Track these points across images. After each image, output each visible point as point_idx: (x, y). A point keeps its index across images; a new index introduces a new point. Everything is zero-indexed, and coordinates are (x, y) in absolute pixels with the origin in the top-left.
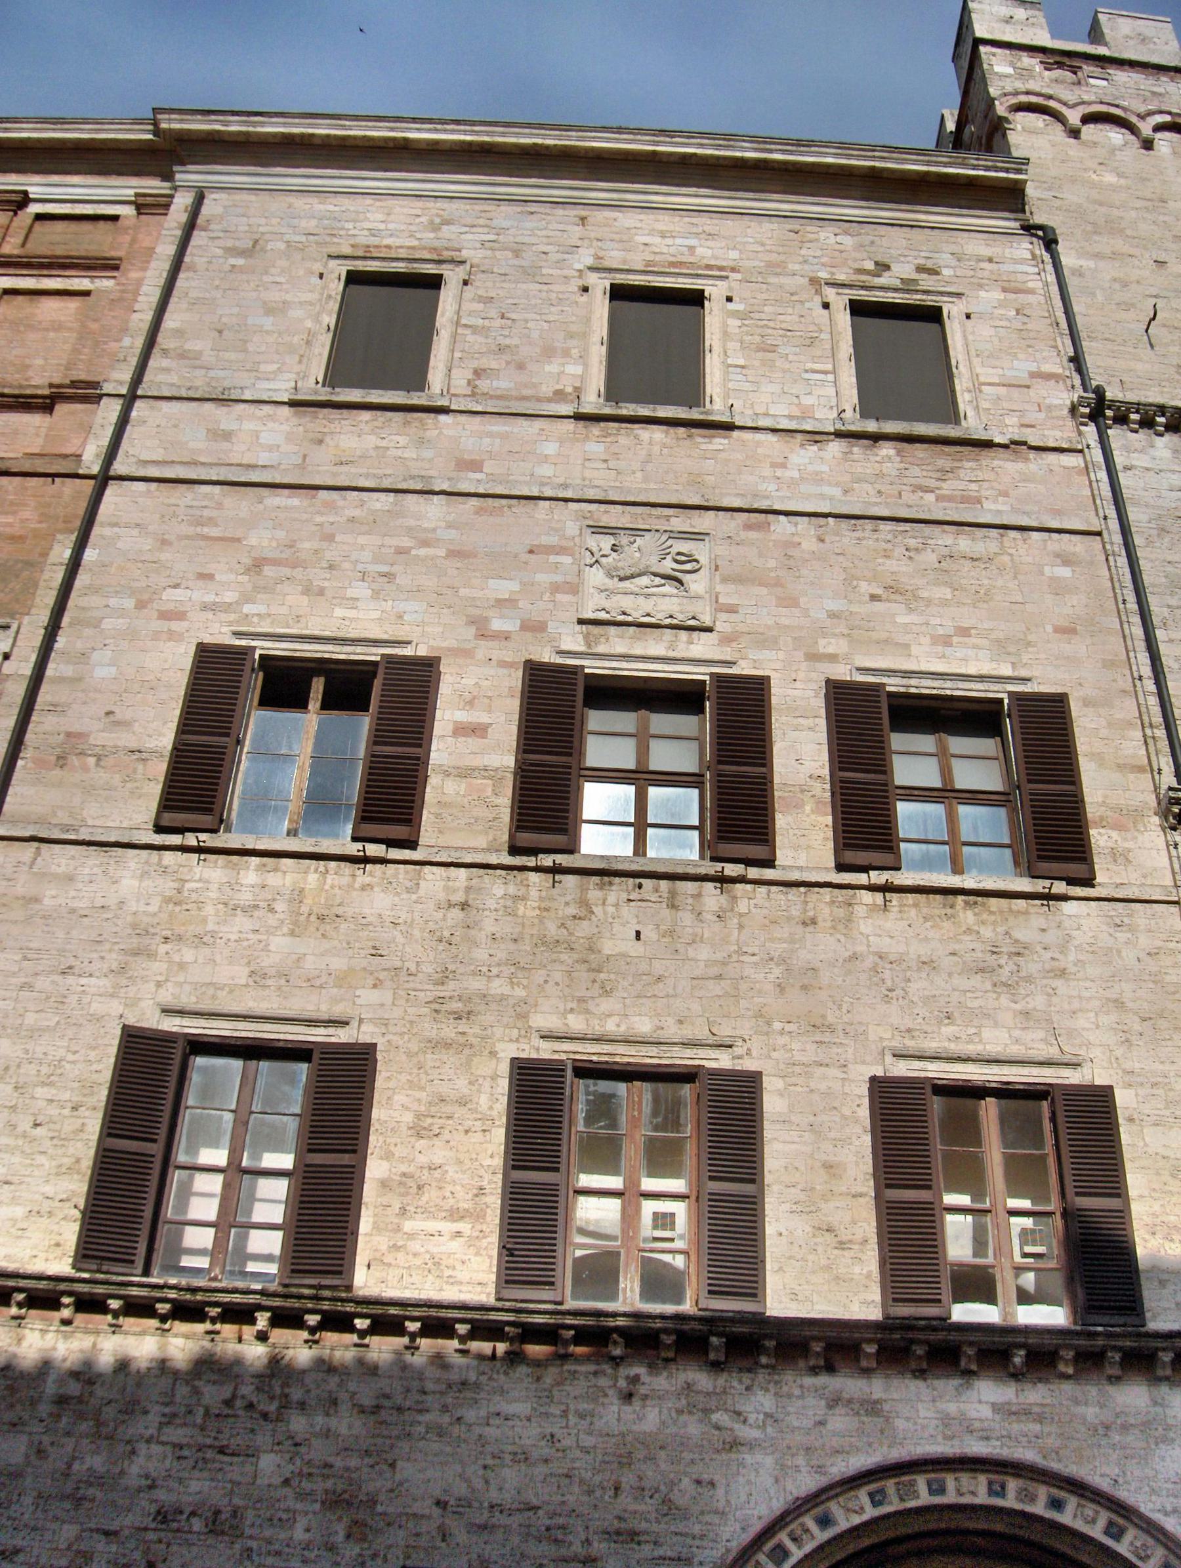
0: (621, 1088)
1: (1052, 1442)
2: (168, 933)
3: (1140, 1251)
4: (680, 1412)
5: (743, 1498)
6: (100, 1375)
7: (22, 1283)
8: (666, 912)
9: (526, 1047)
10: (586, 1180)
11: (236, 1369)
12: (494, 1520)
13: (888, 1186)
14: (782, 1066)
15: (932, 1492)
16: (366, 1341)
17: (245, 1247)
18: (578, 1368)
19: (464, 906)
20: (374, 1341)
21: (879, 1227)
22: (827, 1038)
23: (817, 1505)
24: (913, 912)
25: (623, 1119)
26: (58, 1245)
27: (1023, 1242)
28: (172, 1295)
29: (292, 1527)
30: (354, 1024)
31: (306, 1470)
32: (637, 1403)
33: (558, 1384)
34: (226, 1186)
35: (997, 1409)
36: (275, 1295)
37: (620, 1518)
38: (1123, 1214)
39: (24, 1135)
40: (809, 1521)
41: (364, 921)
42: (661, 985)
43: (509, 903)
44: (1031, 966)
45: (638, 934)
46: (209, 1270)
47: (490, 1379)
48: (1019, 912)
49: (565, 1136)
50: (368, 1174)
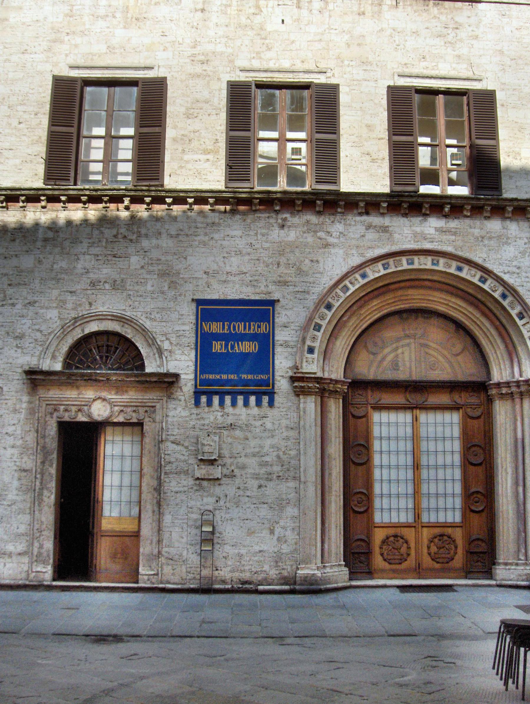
0: (277, 92)
1: (459, 243)
2: (68, 31)
3: (502, 163)
4: (304, 232)
5: (330, 266)
6: (61, 228)
7: (23, 192)
8: (296, 10)
9: (234, 75)
10: (263, 134)
11: (117, 222)
12: (228, 279)
13: (394, 135)
14: (348, 81)
15: (408, 264)
16: (171, 207)
17: (116, 170)
18: (261, 215)
19: (203, 10)
20: (175, 207)
21: (389, 152)
22: (369, 68)
23: (360, 270)
24: (409, 8)
25: (278, 106)
26: (36, 175)
27: (452, 159)
28: (87, 193)
29: (146, 285)
30: (156, 68)
31: (150, 262)
32: (286, 229)
33: (253, 222)
34: (106, 144)
35: (436, 229)
36: (131, 190)
37: (280, 276)
38: (496, 148)
39: (15, 128)
40: (357, 276)
41: (157, 20)
42: (294, 45)
43: (223, 8)
44: (462, 34)
45: (283, 21)
46: (102, 181)
47: (224, 221)
48: (458, 8)
49: (252, 115)
50: (167, 136)
